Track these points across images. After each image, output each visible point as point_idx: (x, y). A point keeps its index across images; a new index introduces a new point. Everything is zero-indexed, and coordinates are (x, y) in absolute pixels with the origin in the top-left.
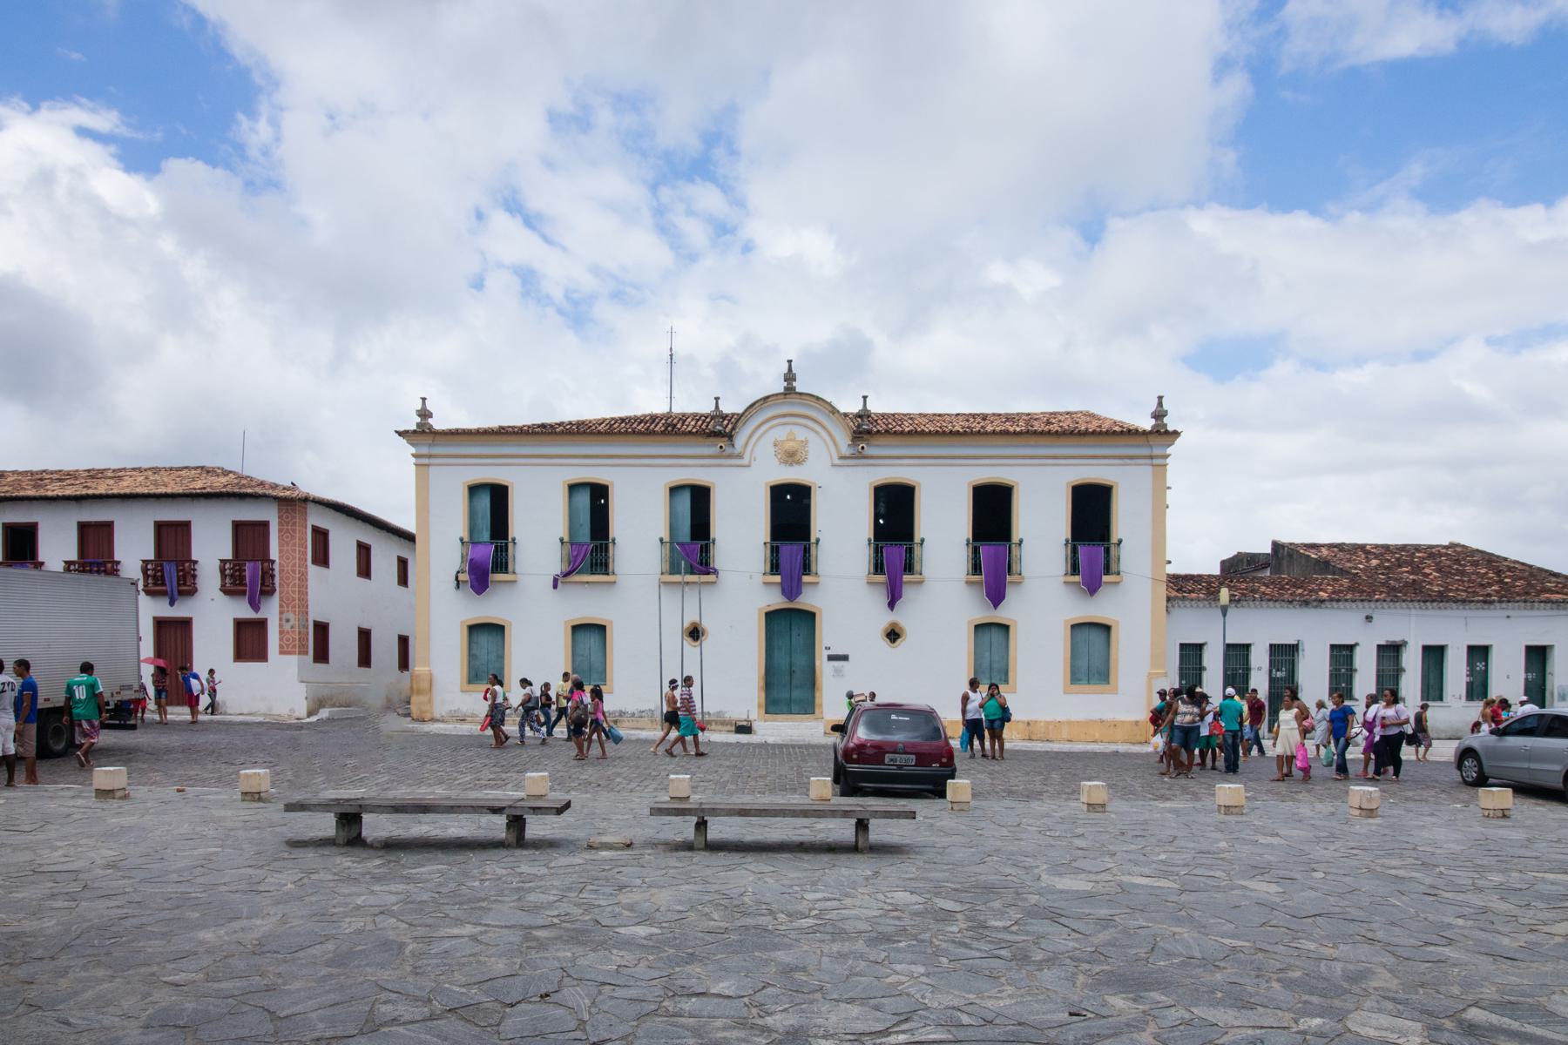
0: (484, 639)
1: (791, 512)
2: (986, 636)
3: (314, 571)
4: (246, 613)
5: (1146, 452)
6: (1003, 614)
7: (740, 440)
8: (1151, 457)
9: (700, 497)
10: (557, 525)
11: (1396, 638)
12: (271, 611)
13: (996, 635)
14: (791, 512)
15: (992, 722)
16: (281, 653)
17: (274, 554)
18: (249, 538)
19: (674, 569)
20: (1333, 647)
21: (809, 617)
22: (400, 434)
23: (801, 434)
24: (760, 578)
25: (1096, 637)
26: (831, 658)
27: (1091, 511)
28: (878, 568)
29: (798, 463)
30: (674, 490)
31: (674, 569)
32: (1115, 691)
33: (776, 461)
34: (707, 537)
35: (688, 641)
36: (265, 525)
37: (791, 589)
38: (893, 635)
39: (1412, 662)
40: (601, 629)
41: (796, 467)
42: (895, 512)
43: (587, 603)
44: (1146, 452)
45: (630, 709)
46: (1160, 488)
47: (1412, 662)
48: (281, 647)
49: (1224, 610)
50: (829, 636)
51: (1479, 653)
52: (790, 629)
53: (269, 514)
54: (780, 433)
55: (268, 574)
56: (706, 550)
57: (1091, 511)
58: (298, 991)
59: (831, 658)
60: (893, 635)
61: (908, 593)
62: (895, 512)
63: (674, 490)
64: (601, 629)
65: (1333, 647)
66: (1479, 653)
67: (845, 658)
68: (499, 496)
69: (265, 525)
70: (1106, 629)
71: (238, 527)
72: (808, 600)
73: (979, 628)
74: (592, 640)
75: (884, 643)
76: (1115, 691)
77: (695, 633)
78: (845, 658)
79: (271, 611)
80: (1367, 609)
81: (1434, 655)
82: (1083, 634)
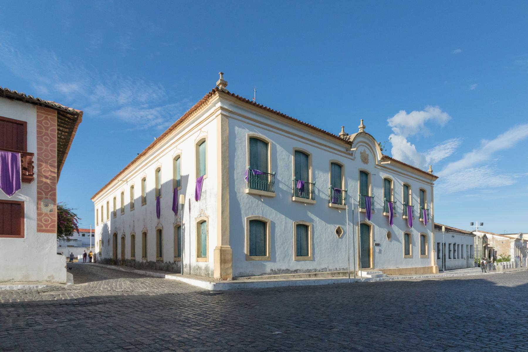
16: (39, 231)
48: (39, 226)
69: (21, 126)
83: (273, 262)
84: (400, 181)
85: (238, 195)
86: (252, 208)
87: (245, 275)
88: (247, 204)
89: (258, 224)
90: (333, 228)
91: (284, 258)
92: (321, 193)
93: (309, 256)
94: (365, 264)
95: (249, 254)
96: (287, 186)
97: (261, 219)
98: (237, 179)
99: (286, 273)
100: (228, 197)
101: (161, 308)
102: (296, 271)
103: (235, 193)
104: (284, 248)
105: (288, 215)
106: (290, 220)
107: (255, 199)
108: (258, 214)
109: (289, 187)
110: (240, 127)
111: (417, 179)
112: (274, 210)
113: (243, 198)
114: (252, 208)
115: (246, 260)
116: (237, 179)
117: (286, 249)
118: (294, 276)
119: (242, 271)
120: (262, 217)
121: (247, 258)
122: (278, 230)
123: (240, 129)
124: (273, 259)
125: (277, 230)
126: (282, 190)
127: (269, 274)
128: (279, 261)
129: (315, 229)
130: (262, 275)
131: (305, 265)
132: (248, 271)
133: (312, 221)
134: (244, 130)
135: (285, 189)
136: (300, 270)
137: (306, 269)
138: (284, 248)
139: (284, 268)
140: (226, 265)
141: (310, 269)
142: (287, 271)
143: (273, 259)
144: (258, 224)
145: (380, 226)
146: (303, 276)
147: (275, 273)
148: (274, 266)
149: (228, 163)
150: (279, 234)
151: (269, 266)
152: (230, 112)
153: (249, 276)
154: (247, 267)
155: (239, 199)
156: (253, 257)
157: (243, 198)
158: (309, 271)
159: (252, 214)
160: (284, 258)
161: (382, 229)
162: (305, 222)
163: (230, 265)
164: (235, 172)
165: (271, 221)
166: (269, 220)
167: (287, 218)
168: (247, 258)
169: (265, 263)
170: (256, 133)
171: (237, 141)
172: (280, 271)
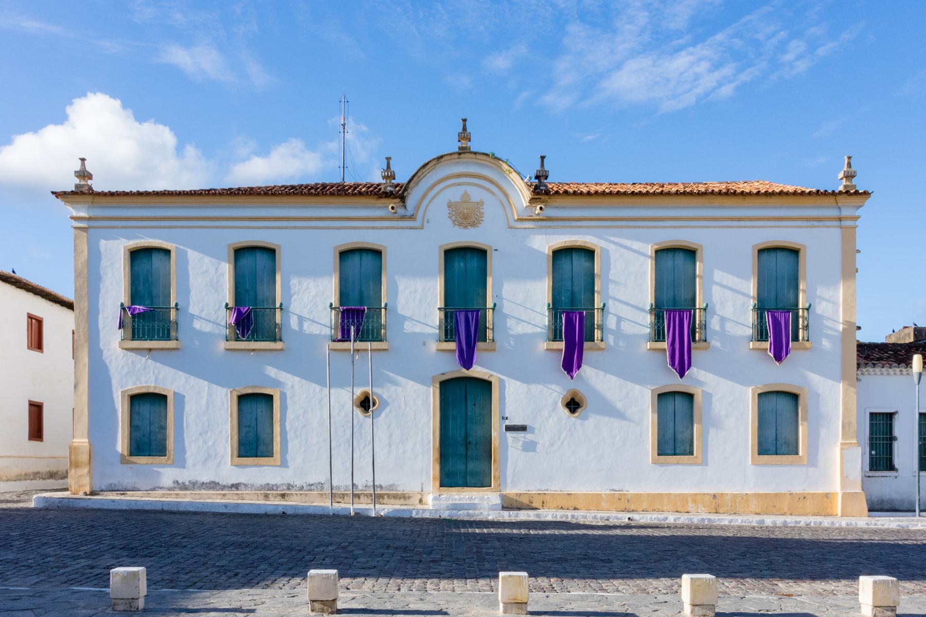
5: (834, 213)
8: (840, 219)
22: (53, 193)
27: (779, 268)
29: (474, 225)
33: (450, 222)
41: (471, 230)
44: (834, 213)
57: (779, 268)
67: (36, 410)
78: (36, 410)
83: (177, 467)
84: (636, 245)
85: (106, 354)
86: (134, 369)
87: (120, 488)
88: (122, 367)
89: (148, 404)
90: (345, 397)
91: (206, 459)
92: (306, 325)
93: (800, 454)
94: (450, 477)
95: (126, 453)
96: (214, 323)
97: (151, 390)
98: (104, 328)
99: (210, 489)
100: (86, 360)
101: (313, 191)
102: (236, 486)
103: (101, 352)
104: (205, 442)
105: (215, 377)
106: (220, 388)
107: (139, 357)
108: (146, 382)
109: (218, 324)
110: (107, 239)
111: (740, 219)
112: (181, 373)
113: (116, 358)
114: (134, 369)
115: (122, 463)
116: (104, 328)
117: (210, 443)
118: (224, 495)
119: (113, 481)
120: (155, 387)
121: (123, 461)
122: (191, 410)
123: (111, 242)
124: (181, 463)
125: (187, 408)
126: (199, 333)
127: (169, 489)
128: (194, 465)
129: (289, 401)
130: (154, 489)
131: (258, 474)
132: (127, 482)
133: (277, 383)
134: (117, 242)
135: (207, 330)
136: (246, 485)
137: (263, 482)
138: (205, 442)
139: (206, 479)
140: (78, 470)
141: (273, 482)
142: (213, 485)
143: (181, 463)
144: (148, 404)
145: (525, 378)
146: (247, 497)
147: (184, 487)
148: (185, 476)
149: (86, 304)
150: (193, 416)
151: (168, 475)
152: (90, 219)
153: (124, 490)
154: (124, 475)
155: (107, 362)
156: (134, 459)
157: (116, 358)
158: (270, 487)
159: (135, 384)
160: (206, 459)
161: (536, 388)
162: (261, 387)
163: (86, 470)
164: (100, 316)
165: (175, 393)
166: (169, 391)
167: (215, 386)
168: (123, 461)
169: (160, 470)
170: (143, 241)
171: (104, 263)
172: (194, 485)
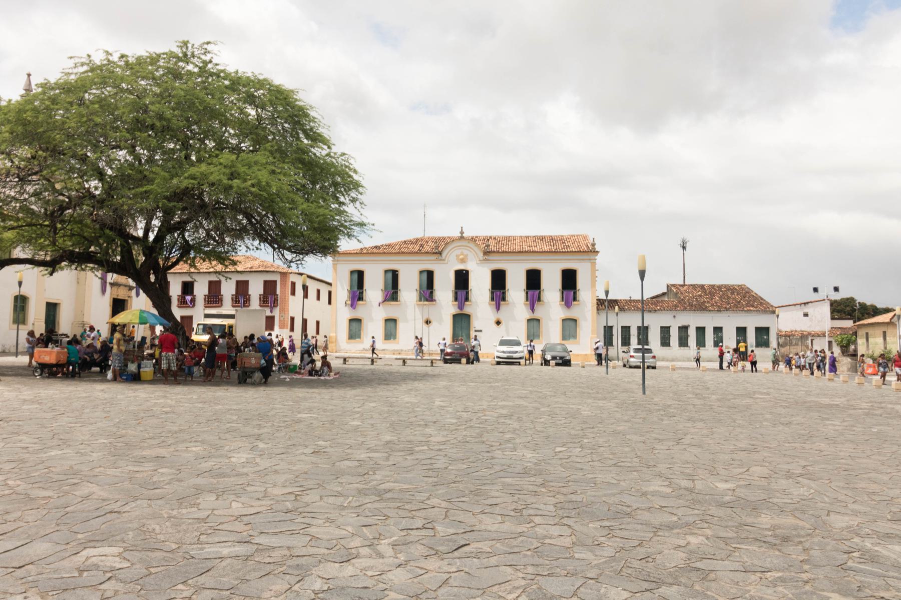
0: (354, 324)
1: (462, 280)
2: (532, 323)
3: (291, 297)
4: (268, 313)
6: (537, 315)
7: (444, 255)
9: (430, 275)
10: (415, 283)
11: (686, 324)
12: (276, 313)
13: (535, 323)
14: (462, 280)
15: (810, 364)
17: (278, 292)
18: (270, 287)
19: (420, 300)
20: (662, 327)
21: (468, 317)
23: (466, 252)
24: (451, 303)
25: (572, 323)
26: (867, 334)
27: (569, 280)
28: (492, 299)
30: (352, 272)
31: (420, 300)
32: (579, 343)
34: (575, 288)
35: (425, 326)
36: (275, 282)
37: (461, 307)
38: (498, 323)
39: (692, 333)
40: (395, 321)
42: (499, 280)
43: (391, 310)
45: (405, 349)
46: (594, 270)
47: (692, 333)
49: (617, 314)
50: (476, 324)
51: (718, 330)
52: (462, 321)
53: (277, 278)
54: (458, 252)
55: (276, 300)
56: (432, 293)
57: (569, 280)
58: (654, 493)
59: (867, 334)
60: (498, 323)
61: (502, 308)
62: (499, 280)
63: (421, 272)
64: (395, 321)
65: (662, 327)
66: (718, 330)
68: (360, 274)
69: (275, 282)
70: (538, 320)
71: (266, 282)
72: (467, 310)
73: (528, 320)
74: (392, 324)
75: (495, 326)
76: (579, 343)
77: (428, 322)
79: (276, 313)
80: (674, 313)
81: (701, 331)
82: (567, 322)
